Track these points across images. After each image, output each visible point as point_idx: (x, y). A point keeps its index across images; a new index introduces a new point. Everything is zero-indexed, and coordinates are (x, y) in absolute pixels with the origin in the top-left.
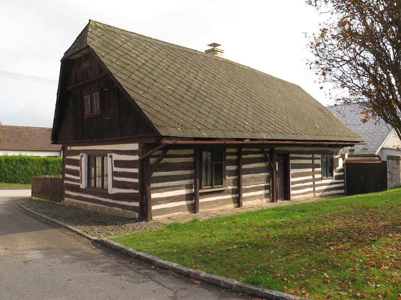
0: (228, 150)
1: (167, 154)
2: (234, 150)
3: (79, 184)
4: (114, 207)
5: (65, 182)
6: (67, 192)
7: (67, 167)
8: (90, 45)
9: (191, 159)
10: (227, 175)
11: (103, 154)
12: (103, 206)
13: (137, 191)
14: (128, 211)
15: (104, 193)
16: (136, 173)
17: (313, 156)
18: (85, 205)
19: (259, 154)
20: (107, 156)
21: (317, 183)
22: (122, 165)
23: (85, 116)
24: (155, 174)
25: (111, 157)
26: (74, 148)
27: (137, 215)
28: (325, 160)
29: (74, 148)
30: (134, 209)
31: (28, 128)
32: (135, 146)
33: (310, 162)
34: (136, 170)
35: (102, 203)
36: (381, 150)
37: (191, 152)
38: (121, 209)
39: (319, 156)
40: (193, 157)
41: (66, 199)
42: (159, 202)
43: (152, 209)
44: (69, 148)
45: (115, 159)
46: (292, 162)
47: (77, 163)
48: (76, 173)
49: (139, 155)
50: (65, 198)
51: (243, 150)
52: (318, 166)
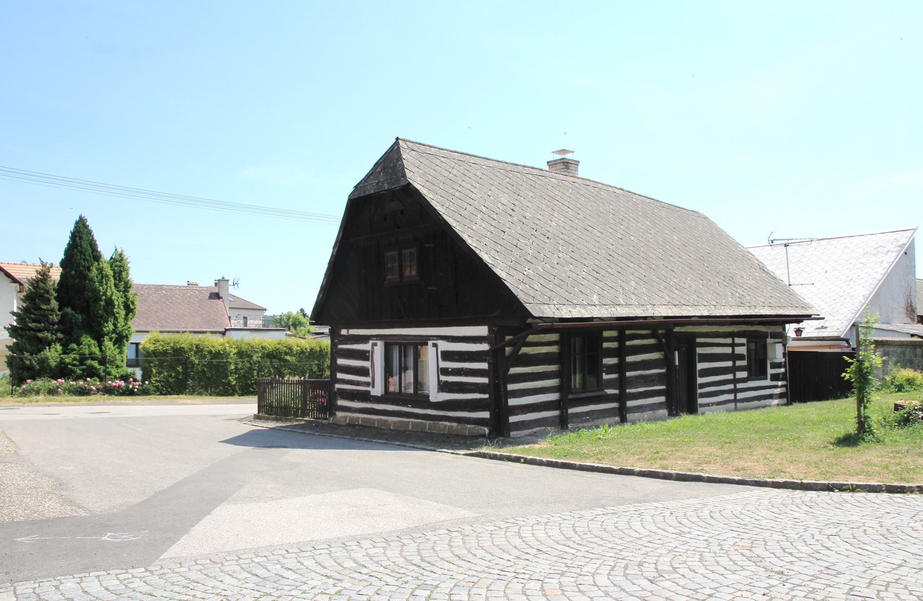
0: (606, 334)
1: (527, 340)
2: (614, 333)
3: (369, 389)
4: (441, 421)
5: (337, 386)
6: (341, 403)
7: (340, 361)
8: (411, 182)
9: (554, 349)
10: (604, 372)
11: (423, 341)
12: (420, 421)
13: (486, 396)
14: (469, 426)
15: (424, 401)
16: (339, 372)
17: (733, 340)
18: (379, 421)
19: (650, 338)
20: (427, 344)
21: (739, 386)
22: (457, 357)
23: (386, 283)
24: (513, 370)
25: (435, 345)
26: (354, 332)
27: (487, 430)
28: (753, 346)
29: (354, 332)
30: (481, 422)
31: (159, 288)
32: (482, 331)
33: (728, 350)
34: (484, 366)
35: (416, 416)
36: (851, 328)
37: (554, 337)
38: (454, 424)
39: (744, 341)
40: (558, 345)
41: (340, 414)
42: (516, 412)
43: (569, 412)
44: (344, 332)
45: (443, 350)
46: (699, 350)
47: (363, 355)
48: (364, 372)
49: (489, 343)
50: (337, 413)
51: (628, 332)
52: (741, 357)
